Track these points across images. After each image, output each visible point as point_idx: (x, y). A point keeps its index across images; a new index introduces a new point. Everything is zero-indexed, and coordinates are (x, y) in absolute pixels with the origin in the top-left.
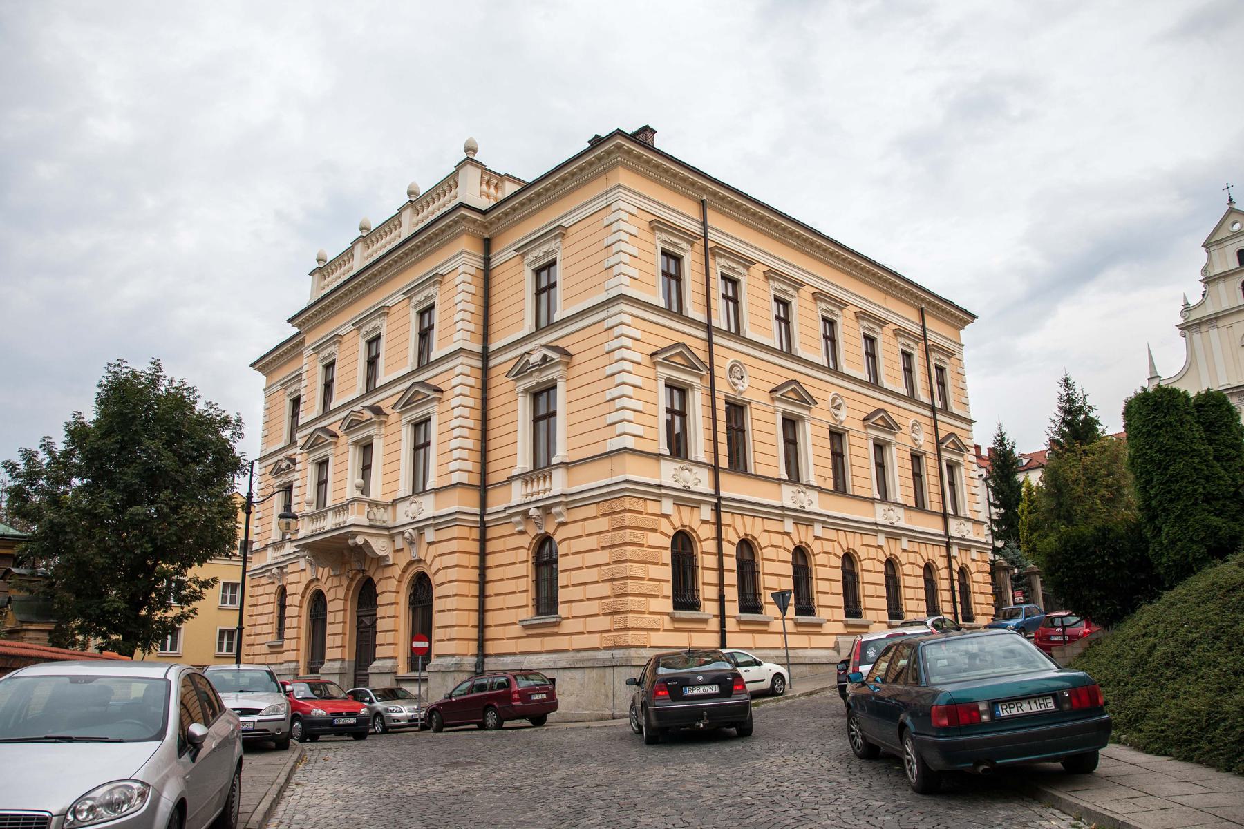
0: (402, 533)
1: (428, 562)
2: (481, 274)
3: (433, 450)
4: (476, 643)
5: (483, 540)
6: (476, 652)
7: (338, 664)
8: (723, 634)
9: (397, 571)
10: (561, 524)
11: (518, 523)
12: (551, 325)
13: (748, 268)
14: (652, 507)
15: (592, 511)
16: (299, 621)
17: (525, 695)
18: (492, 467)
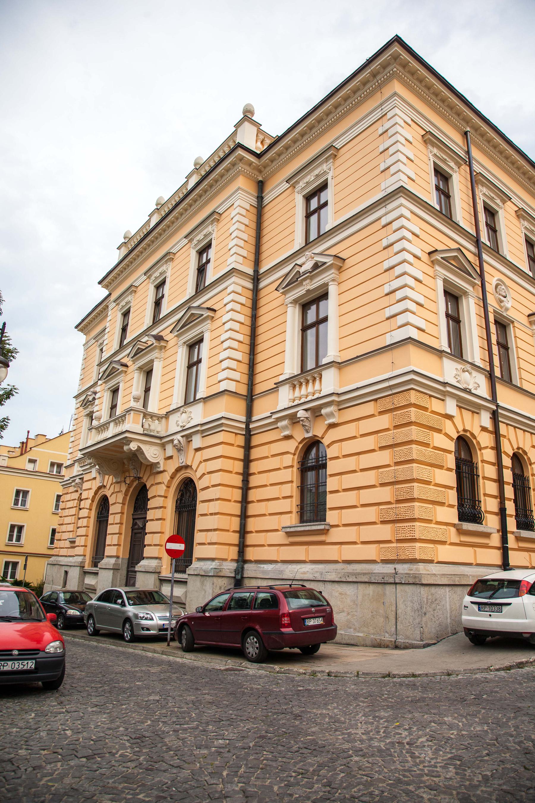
0: (172, 441)
1: (194, 467)
2: (254, 211)
3: (203, 367)
4: (236, 549)
5: (248, 447)
6: (236, 557)
7: (113, 561)
8: (505, 551)
9: (166, 477)
10: (332, 426)
11: (285, 428)
12: (321, 237)
13: (504, 202)
14: (436, 405)
15: (369, 409)
16: (88, 522)
17: (297, 619)
18: (258, 378)
